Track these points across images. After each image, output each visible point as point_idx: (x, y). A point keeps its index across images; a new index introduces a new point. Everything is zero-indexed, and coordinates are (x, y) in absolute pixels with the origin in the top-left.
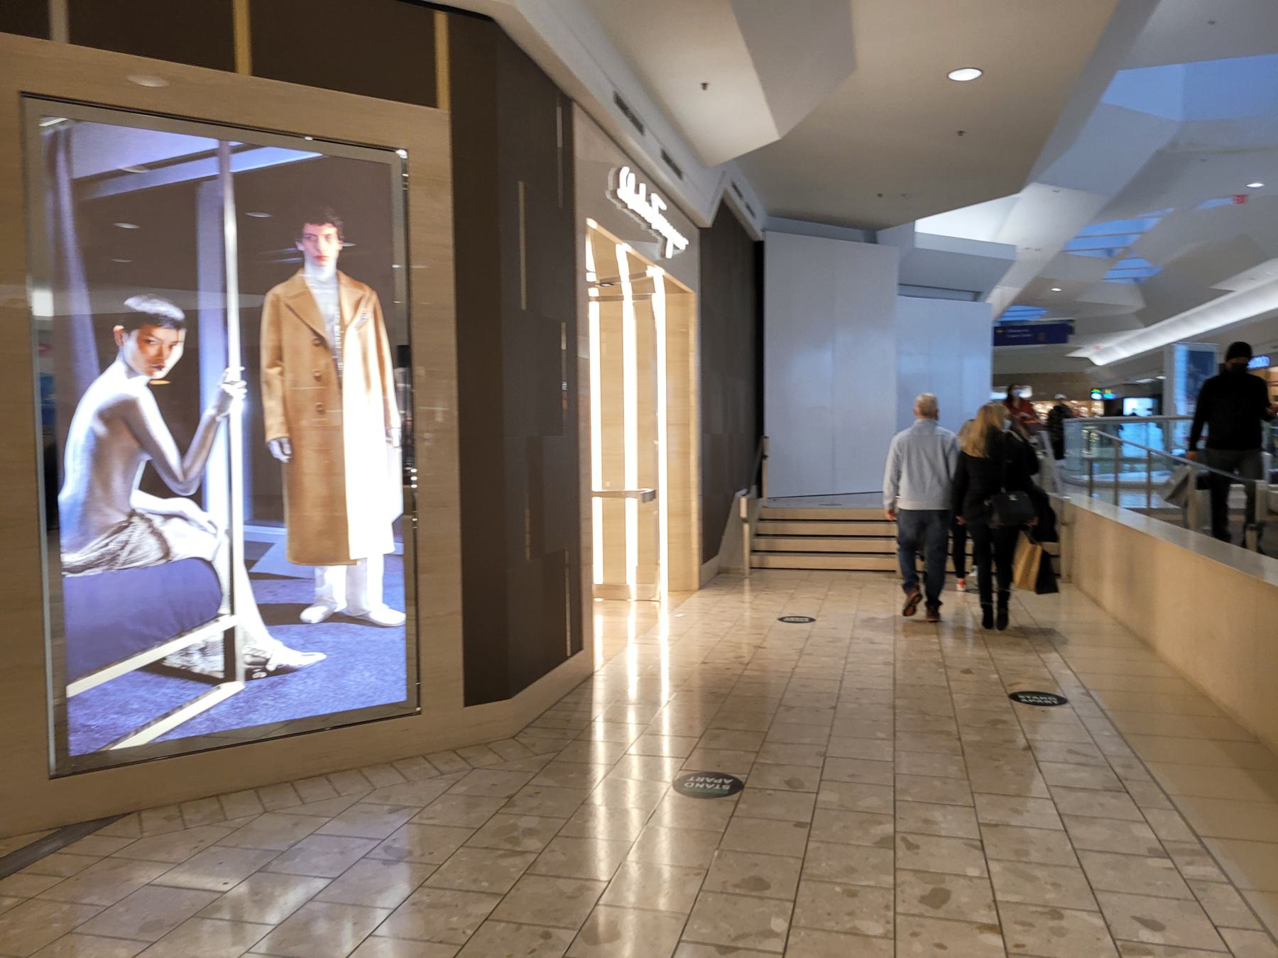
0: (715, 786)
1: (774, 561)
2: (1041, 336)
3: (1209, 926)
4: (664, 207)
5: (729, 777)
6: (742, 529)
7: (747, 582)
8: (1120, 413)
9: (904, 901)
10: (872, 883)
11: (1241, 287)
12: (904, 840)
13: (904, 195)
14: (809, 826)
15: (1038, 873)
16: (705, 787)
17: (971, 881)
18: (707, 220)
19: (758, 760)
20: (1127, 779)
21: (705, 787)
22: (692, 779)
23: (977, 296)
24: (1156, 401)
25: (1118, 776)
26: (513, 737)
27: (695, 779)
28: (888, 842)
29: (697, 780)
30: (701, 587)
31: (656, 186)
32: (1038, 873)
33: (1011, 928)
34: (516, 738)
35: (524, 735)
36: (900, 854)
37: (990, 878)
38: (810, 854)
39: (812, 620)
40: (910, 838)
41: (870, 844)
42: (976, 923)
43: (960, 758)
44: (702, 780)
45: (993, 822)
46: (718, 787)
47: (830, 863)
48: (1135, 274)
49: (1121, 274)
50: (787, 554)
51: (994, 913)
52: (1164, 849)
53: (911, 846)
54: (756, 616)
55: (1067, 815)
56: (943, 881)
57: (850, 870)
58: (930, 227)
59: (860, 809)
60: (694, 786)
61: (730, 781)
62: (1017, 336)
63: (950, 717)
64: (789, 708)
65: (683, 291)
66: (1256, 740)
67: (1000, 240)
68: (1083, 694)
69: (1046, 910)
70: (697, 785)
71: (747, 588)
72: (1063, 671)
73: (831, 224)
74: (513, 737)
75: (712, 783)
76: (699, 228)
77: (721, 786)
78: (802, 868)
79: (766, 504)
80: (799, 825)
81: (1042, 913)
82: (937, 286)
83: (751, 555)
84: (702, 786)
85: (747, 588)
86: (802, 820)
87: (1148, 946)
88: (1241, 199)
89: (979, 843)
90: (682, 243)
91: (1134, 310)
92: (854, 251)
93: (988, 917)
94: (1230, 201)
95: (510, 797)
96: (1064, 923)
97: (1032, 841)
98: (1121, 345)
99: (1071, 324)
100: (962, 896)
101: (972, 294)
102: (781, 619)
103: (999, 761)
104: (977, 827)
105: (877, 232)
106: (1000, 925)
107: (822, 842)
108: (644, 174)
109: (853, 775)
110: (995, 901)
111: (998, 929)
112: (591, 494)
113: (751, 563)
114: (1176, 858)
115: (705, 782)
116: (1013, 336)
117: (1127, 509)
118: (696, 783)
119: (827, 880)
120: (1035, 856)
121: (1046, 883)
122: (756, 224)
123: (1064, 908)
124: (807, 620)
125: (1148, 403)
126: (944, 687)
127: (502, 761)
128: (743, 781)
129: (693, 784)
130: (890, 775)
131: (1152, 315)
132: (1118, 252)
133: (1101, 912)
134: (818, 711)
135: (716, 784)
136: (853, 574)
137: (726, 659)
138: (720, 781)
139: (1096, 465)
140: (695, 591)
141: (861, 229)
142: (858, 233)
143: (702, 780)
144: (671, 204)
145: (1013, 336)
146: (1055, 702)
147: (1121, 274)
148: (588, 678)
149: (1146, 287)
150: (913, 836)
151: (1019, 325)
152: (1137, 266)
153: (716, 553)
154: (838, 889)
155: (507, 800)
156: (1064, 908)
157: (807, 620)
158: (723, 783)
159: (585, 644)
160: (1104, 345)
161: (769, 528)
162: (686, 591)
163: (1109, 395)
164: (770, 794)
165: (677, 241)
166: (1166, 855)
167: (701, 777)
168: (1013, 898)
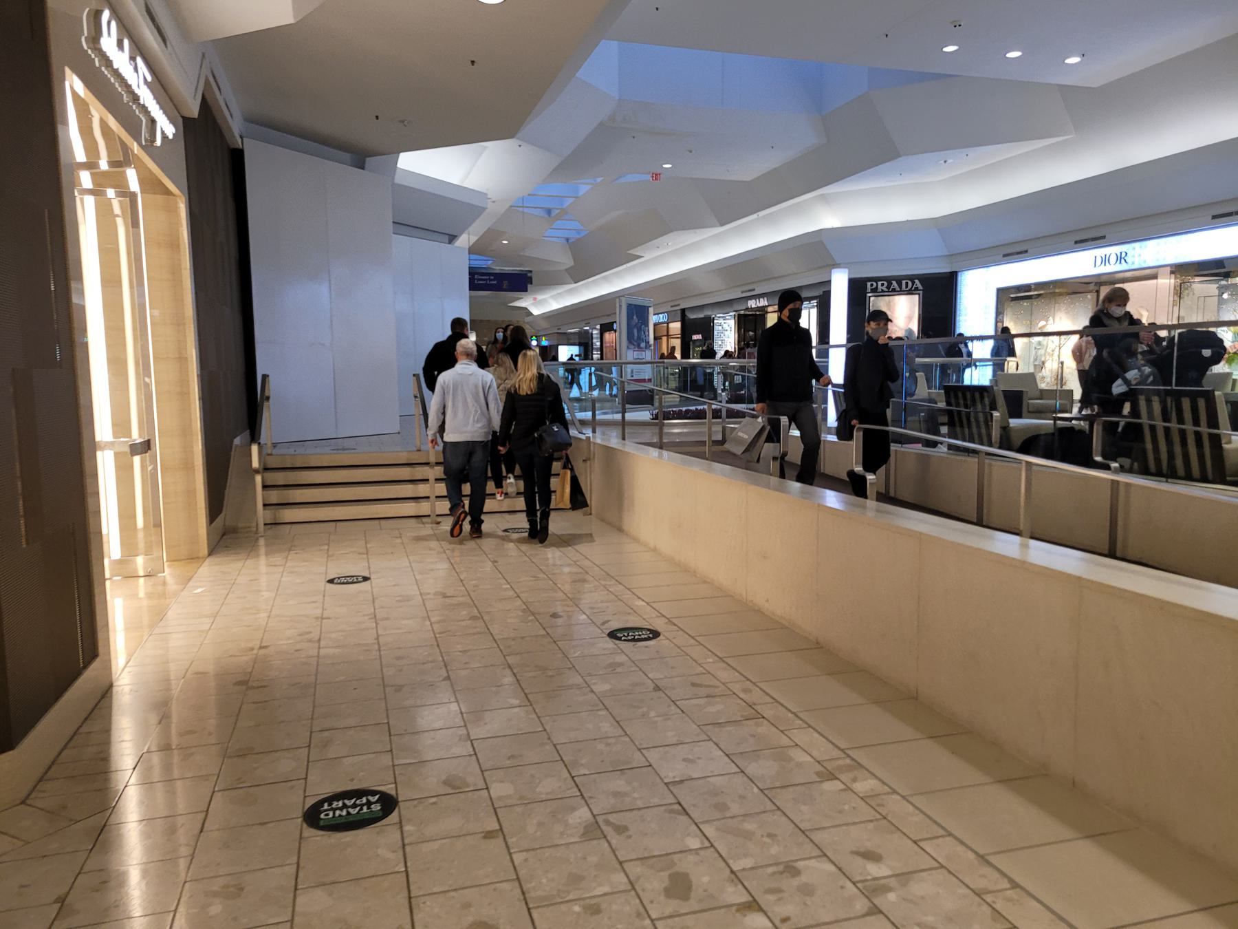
0: (361, 809)
1: (289, 515)
2: (505, 284)
3: (909, 842)
4: (149, 79)
5: (374, 793)
6: (254, 480)
7: (262, 542)
8: (555, 358)
9: (652, 902)
10: (607, 889)
11: (648, 253)
12: (608, 822)
13: (403, 122)
14: (500, 833)
15: (749, 826)
16: (348, 813)
17: (697, 854)
18: (194, 111)
19: (396, 762)
20: (755, 704)
21: (348, 813)
22: (326, 806)
23: (452, 238)
24: (582, 348)
25: (746, 703)
26: (23, 802)
27: (329, 806)
28: (593, 831)
29: (334, 806)
30: (210, 554)
31: (139, 49)
32: (749, 826)
33: (766, 900)
34: (28, 802)
35: (42, 795)
36: (614, 842)
37: (712, 846)
38: (522, 873)
39: (366, 579)
40: (612, 818)
41: (577, 839)
42: (734, 905)
43: (604, 713)
44: (340, 804)
45: (677, 779)
46: (365, 809)
47: (550, 875)
48: (567, 234)
49: (554, 233)
50: (320, 505)
51: (740, 886)
52: (828, 770)
53: (621, 830)
54: (298, 581)
55: (731, 754)
56: (673, 864)
57: (576, 880)
58: (414, 163)
59: (543, 797)
60: (334, 816)
61: (378, 796)
62: (484, 282)
63: (570, 668)
64: (399, 688)
65: (168, 192)
66: (818, 646)
67: (467, 184)
68: (666, 623)
69: (781, 868)
70: (338, 813)
71: (262, 550)
72: (637, 603)
73: (315, 141)
74: (23, 802)
75: (354, 806)
76: (183, 117)
77: (368, 808)
78: (523, 893)
79: (269, 452)
80: (489, 835)
81: (782, 873)
82: (404, 223)
83: (264, 509)
84: (344, 813)
85: (262, 550)
86: (489, 829)
87: (882, 882)
88: (656, 176)
89: (677, 807)
90: (170, 131)
91: (568, 267)
92: (338, 172)
93: (736, 895)
94: (649, 177)
95: (61, 900)
96: (804, 878)
97: (722, 792)
98: (554, 297)
99: (529, 275)
100: (703, 877)
101: (447, 236)
102: (331, 581)
103: (641, 708)
104: (666, 788)
105: (368, 159)
106: (755, 900)
107: (527, 851)
108: (126, 30)
109: (512, 757)
110: (732, 872)
111: (753, 906)
112: (94, 447)
113: (264, 518)
114: (843, 777)
115: (345, 806)
116: (481, 282)
117: (638, 443)
118: (334, 810)
119: (559, 900)
120: (735, 808)
121: (762, 836)
122: (235, 125)
123: (797, 861)
124: (360, 579)
125: (575, 350)
126: (543, 636)
127: (19, 843)
128: (393, 793)
129: (331, 814)
130: (549, 747)
131: (580, 272)
132: (554, 213)
133: (825, 855)
134: (644, 715)
135: (362, 805)
136: (383, 522)
137: (289, 638)
138: (364, 800)
139: (597, 405)
140: (204, 559)
141: (348, 152)
142: (347, 156)
143: (340, 804)
144: (155, 78)
145: (481, 282)
146: (651, 636)
147: (554, 233)
148: (106, 692)
149: (574, 246)
150: (614, 815)
151: (484, 271)
152: (569, 228)
153: (220, 512)
154: (577, 908)
155: (59, 905)
156: (797, 861)
157: (360, 579)
158: (369, 804)
159: (101, 650)
160: (540, 297)
161: (280, 478)
162: (192, 559)
163: (544, 343)
164: (434, 803)
165: (166, 127)
166: (832, 777)
167: (338, 801)
168: (748, 862)
